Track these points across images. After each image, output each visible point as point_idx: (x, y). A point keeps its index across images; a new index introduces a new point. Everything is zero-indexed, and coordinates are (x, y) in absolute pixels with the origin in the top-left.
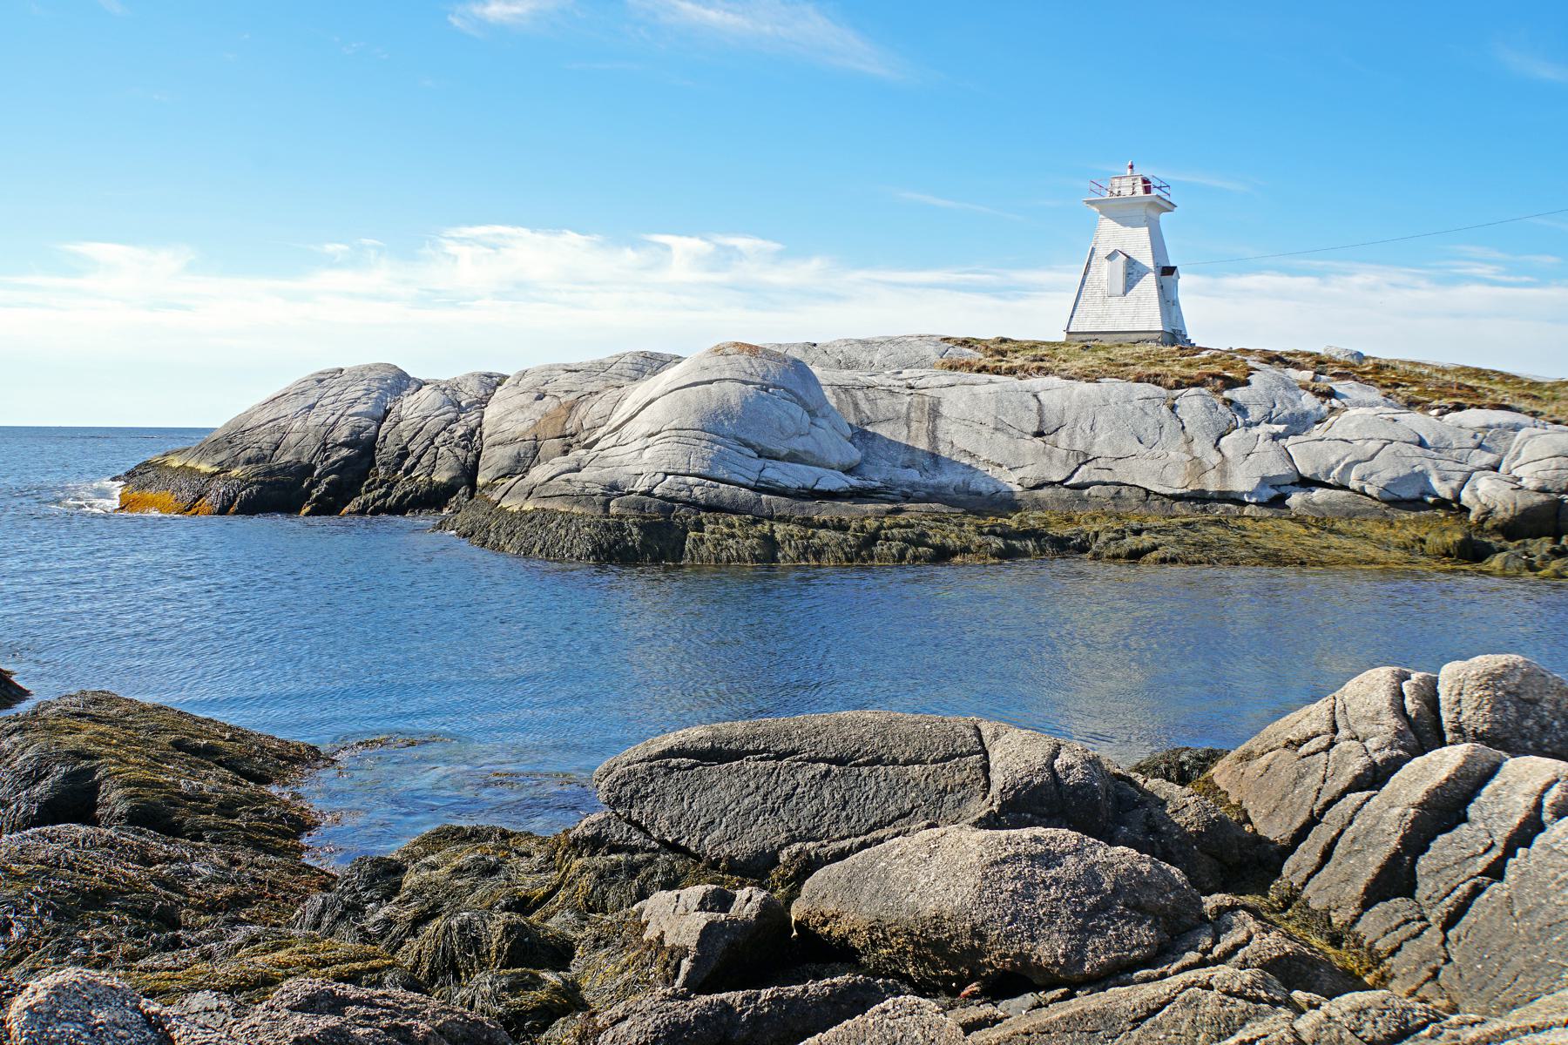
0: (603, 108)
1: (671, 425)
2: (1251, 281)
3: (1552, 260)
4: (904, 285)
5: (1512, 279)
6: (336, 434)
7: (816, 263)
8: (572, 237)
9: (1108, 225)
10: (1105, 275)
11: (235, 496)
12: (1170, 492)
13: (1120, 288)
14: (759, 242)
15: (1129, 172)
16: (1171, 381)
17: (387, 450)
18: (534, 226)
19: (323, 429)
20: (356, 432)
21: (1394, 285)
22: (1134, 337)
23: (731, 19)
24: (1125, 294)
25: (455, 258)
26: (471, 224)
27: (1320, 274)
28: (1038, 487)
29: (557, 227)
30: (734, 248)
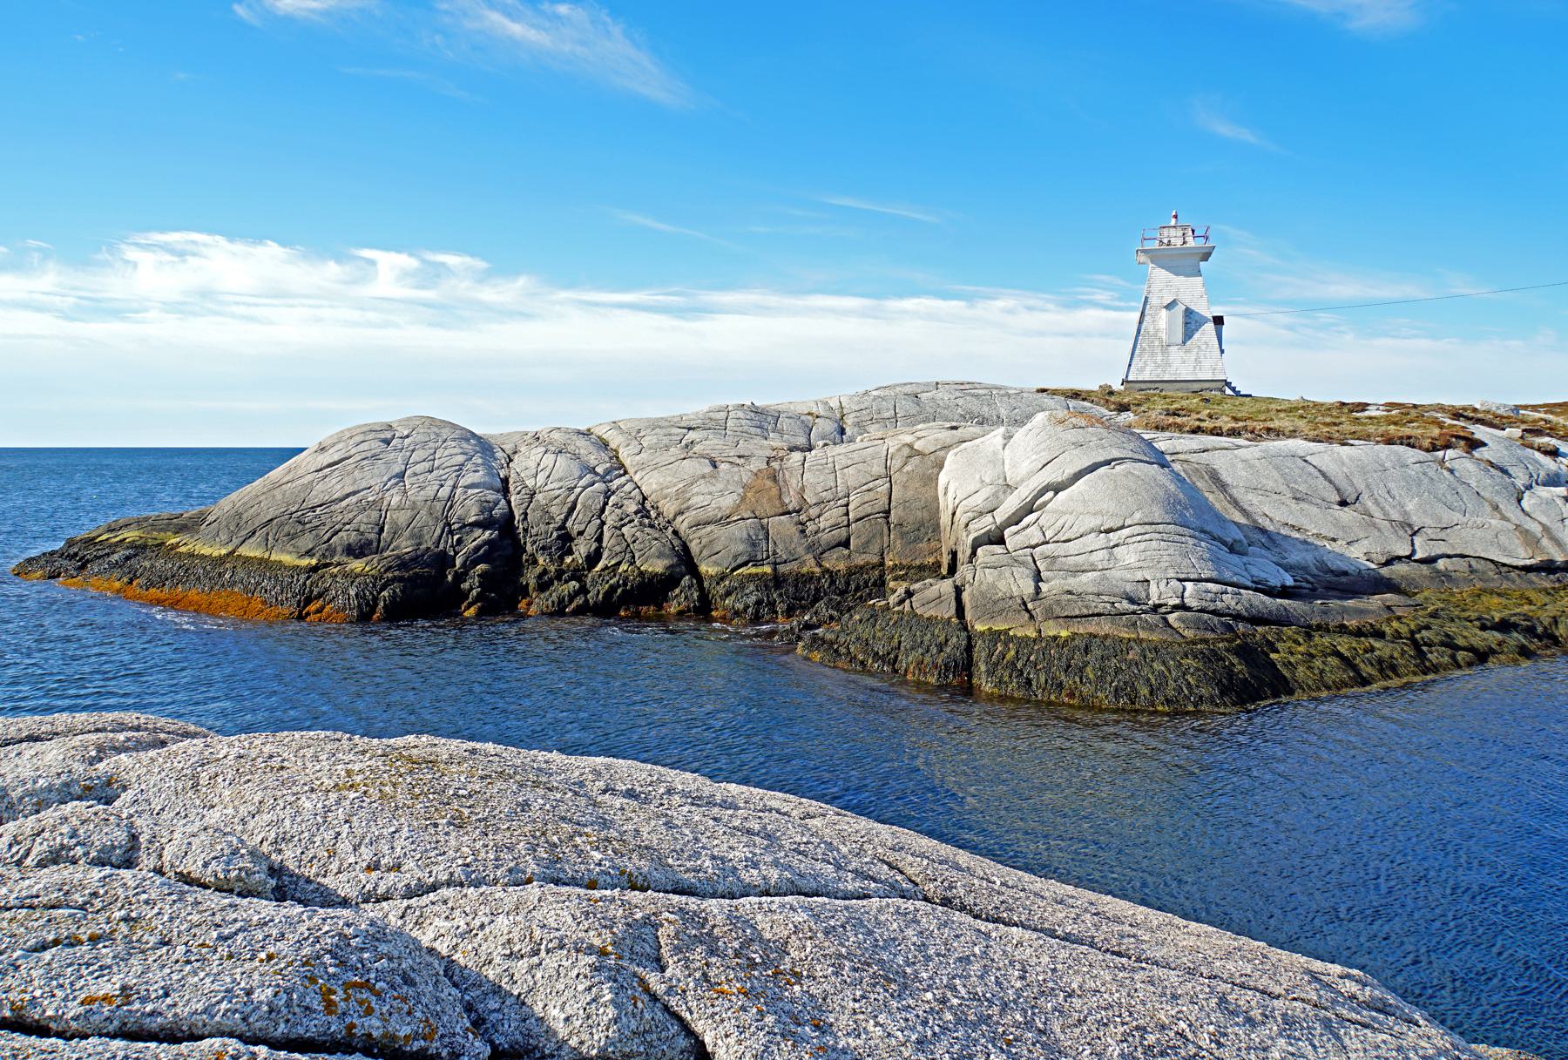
0: (379, 111)
1: (1138, 516)
2: (910, 304)
4: (596, 304)
6: (458, 511)
7: (522, 281)
8: (273, 249)
9: (1160, 275)
11: (376, 599)
12: (1521, 563)
13: (1179, 337)
14: (468, 259)
15: (1173, 222)
16: (1426, 443)
17: (535, 535)
18: (231, 237)
19: (439, 506)
20: (486, 507)
21: (1030, 309)
23: (533, 35)
24: (1184, 343)
25: (135, 265)
26: (163, 230)
27: (969, 298)
28: (1388, 563)
29: (259, 239)
30: (443, 264)
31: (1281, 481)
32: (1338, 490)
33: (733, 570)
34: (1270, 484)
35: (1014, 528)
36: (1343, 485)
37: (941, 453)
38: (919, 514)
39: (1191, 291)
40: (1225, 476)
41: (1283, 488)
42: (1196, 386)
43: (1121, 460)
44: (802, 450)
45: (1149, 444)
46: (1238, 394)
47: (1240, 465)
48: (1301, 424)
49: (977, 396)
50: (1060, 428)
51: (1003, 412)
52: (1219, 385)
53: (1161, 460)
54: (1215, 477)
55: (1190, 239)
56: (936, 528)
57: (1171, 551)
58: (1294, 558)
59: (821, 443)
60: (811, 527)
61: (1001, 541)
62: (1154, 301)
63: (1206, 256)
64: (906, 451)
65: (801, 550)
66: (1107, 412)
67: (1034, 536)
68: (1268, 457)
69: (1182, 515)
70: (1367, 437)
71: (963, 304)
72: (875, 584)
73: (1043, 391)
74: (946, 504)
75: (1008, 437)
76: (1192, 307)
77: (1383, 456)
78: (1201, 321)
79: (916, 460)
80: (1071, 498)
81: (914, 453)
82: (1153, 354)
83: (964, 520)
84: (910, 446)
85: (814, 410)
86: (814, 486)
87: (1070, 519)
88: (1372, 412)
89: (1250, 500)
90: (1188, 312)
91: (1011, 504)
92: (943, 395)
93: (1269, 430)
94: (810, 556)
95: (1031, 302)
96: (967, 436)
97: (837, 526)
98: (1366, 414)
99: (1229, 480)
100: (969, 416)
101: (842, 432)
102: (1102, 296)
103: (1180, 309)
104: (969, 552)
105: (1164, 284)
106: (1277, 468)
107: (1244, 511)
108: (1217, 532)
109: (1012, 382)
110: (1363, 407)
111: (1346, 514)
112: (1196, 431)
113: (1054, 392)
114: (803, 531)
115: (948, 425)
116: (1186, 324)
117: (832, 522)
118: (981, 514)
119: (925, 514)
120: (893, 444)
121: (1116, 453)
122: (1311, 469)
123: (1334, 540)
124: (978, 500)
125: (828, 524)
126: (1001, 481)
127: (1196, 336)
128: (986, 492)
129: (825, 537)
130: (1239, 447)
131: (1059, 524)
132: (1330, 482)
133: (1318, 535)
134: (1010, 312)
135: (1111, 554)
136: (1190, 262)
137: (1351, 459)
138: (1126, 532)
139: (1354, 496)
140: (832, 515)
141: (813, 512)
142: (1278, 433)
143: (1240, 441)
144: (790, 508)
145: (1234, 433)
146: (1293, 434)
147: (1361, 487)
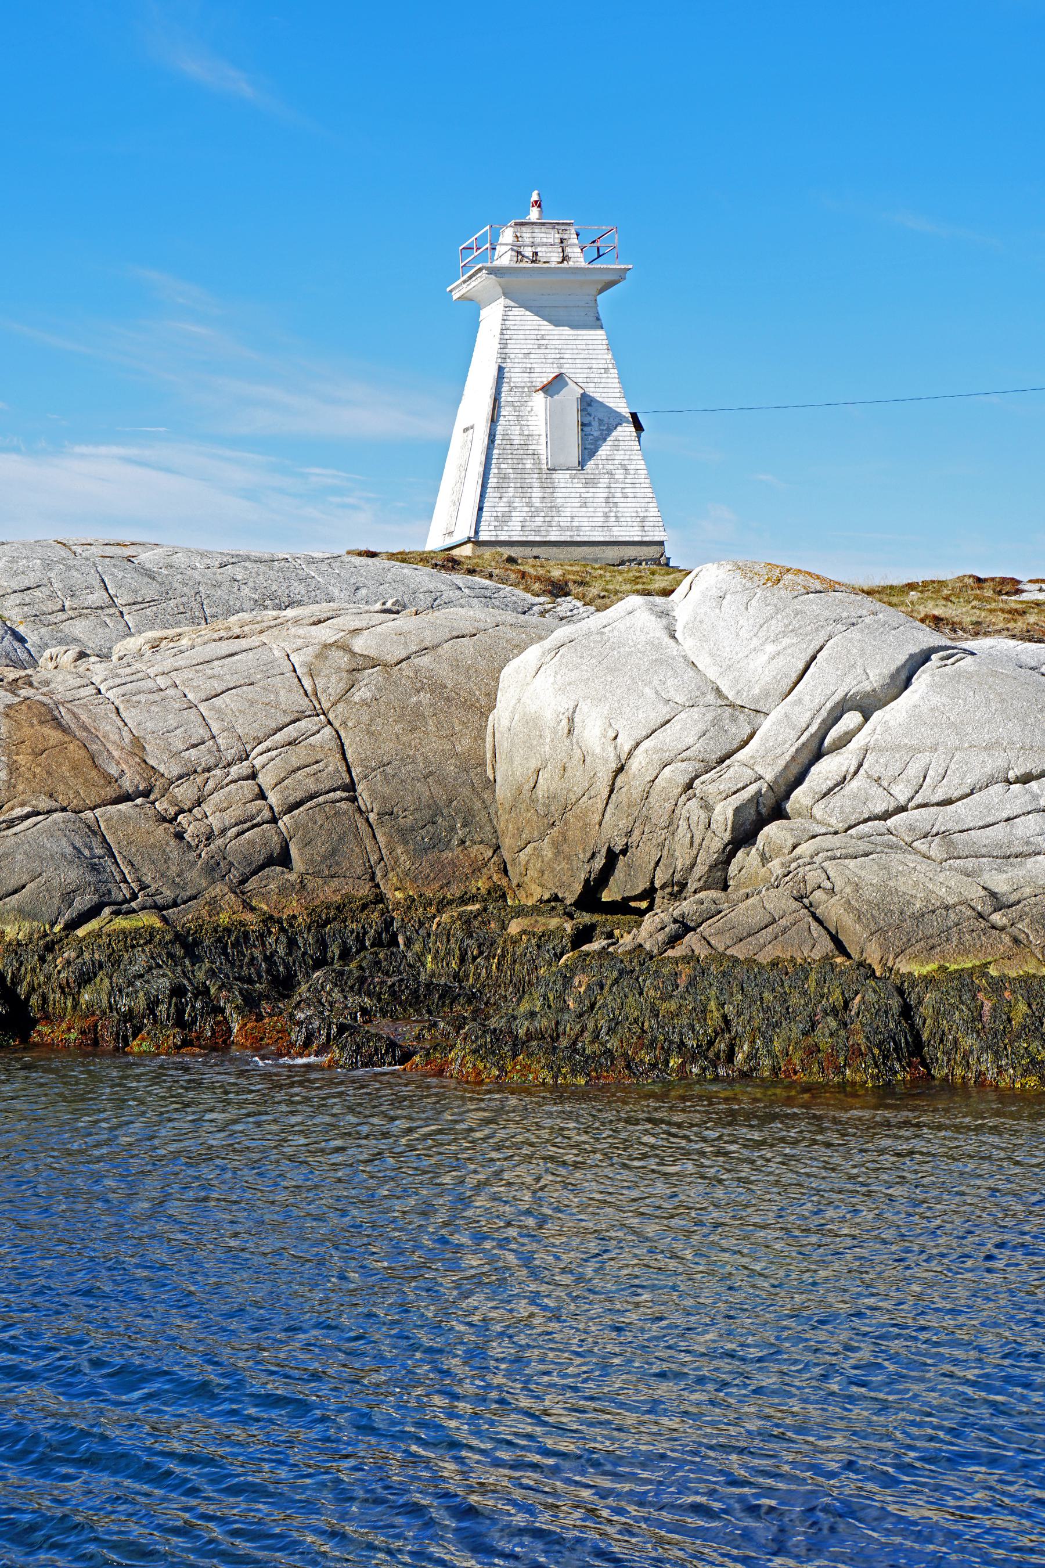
13: (573, 455)
15: (534, 215)
22: (612, 554)
24: (582, 464)
33: (73, 925)
55: (574, 252)
62: (515, 376)
64: (343, 660)
65: (195, 877)
72: (377, 943)
76: (592, 392)
78: (610, 421)
82: (524, 489)
90: (586, 402)
97: (247, 823)
103: (571, 394)
110: (1010, 586)
114: (179, 836)
117: (235, 813)
125: (229, 817)
127: (604, 451)
131: (914, 770)
141: (185, 792)
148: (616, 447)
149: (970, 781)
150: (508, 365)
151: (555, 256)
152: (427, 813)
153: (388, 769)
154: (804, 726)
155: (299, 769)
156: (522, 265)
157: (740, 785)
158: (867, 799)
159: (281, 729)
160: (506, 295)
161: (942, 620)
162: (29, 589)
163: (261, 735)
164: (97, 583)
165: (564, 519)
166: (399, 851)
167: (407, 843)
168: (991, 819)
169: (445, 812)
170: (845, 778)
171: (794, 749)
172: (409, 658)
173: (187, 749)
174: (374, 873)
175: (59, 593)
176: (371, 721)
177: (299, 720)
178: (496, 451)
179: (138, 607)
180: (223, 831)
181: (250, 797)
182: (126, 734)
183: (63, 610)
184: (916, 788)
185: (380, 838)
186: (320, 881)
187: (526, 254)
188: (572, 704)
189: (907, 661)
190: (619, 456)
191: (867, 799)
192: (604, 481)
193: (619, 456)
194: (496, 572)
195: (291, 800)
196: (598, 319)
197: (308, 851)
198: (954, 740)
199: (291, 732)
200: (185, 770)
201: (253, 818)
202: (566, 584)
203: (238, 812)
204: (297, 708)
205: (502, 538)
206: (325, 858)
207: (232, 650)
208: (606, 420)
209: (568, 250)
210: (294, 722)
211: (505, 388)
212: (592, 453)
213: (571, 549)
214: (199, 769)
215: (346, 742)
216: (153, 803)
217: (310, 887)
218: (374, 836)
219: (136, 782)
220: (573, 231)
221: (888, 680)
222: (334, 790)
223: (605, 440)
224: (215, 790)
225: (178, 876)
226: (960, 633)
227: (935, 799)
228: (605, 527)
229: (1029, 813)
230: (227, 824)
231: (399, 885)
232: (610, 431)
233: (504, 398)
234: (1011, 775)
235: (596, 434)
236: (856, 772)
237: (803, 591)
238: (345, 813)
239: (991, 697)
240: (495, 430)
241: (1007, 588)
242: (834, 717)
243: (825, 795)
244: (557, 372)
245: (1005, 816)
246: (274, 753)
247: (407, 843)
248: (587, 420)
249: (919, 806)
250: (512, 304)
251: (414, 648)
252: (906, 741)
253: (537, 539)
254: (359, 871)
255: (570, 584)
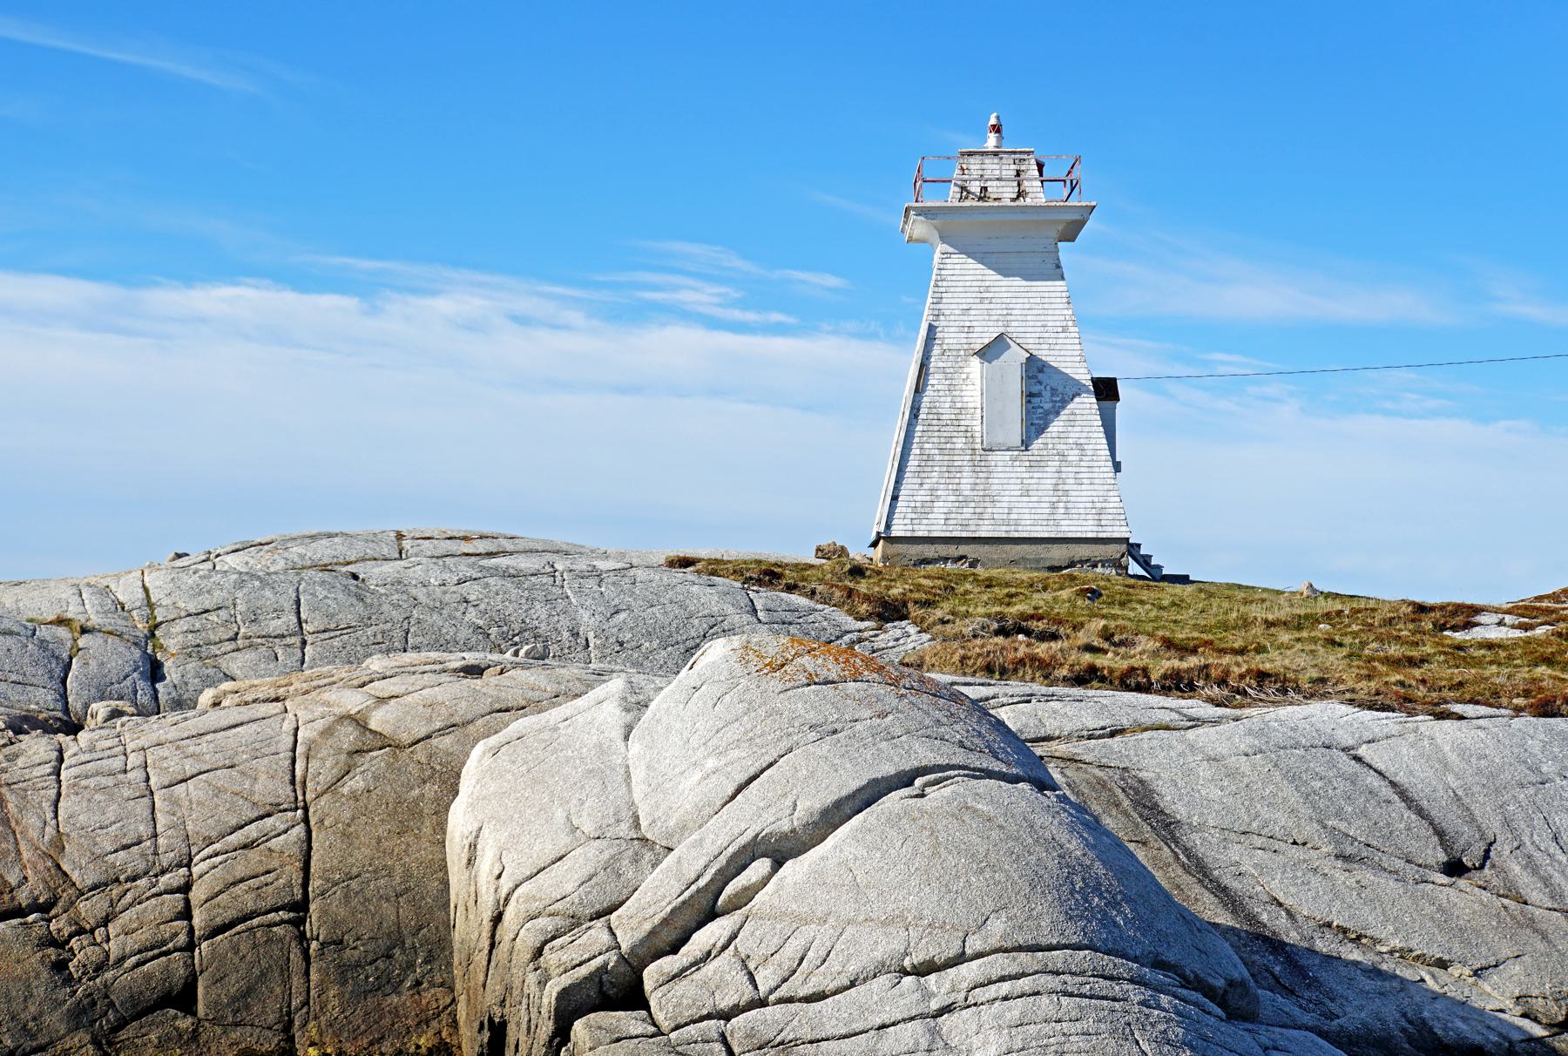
1: (997, 928)
3: (832, 281)
5: (751, 316)
9: (962, 274)
10: (972, 395)
13: (1015, 434)
15: (991, 141)
21: (522, 321)
24: (1026, 444)
27: (366, 289)
31: (1305, 811)
32: (1440, 834)
34: (1281, 821)
35: (669, 964)
36: (1451, 820)
37: (446, 742)
38: (387, 909)
39: (1042, 317)
40: (1168, 798)
41: (1310, 830)
42: (1058, 554)
43: (938, 772)
44: (47, 728)
45: (979, 708)
46: (1155, 575)
47: (1205, 771)
48: (1334, 659)
49: (506, 574)
50: (774, 683)
51: (587, 622)
52: (1114, 551)
53: (1024, 763)
54: (1144, 801)
55: (1032, 185)
56: (439, 947)
57: (1088, 1024)
58: (1355, 1014)
59: (100, 709)
60: (83, 953)
61: (630, 996)
62: (949, 337)
63: (1071, 232)
64: (348, 736)
66: (850, 623)
67: (724, 982)
68: (1270, 749)
69: (1107, 923)
70: (1492, 698)
71: (349, 303)
73: (685, 563)
74: (472, 888)
75: (636, 705)
76: (1043, 354)
77: (1535, 746)
78: (1065, 392)
79: (377, 760)
80: (817, 877)
81: (372, 742)
82: (951, 470)
83: (529, 938)
84: (359, 721)
85: (72, 612)
86: (89, 833)
87: (821, 937)
88: (1488, 630)
89: (1237, 861)
90: (1035, 369)
91: (656, 894)
92: (421, 571)
93: (1262, 676)
94: (83, 1036)
95: (524, 305)
96: (513, 697)
97: (157, 948)
98: (1477, 634)
99: (1180, 811)
100: (504, 634)
101: (155, 672)
102: (699, 296)
103: (1014, 359)
104: (546, 1028)
105: (971, 295)
106: (1293, 778)
107: (1222, 892)
108: (1193, 966)
109: (608, 542)
110: (1466, 615)
111: (1463, 897)
112: (1086, 677)
113: (715, 568)
114: (60, 966)
115: (455, 660)
116: (1030, 396)
117: (143, 936)
118: (575, 922)
119: (406, 912)
120: (309, 715)
121: (924, 754)
122: (1372, 780)
123: (1443, 964)
124: (564, 882)
125: (132, 943)
126: (624, 829)
127: (1055, 427)
128: (585, 859)
129: (122, 980)
130: (1196, 722)
132: (1421, 812)
133: (1404, 954)
134: (473, 326)
135: (934, 1032)
136: (1028, 243)
137: (1462, 752)
138: (969, 972)
139: (1478, 849)
140: (139, 922)
141: (90, 909)
142: (1281, 686)
143: (1197, 707)
144: (23, 897)
145: (1178, 684)
146: (1319, 689)
147: (1494, 826)
148: (1071, 423)
149: (853, 968)
150: (941, 323)
151: (1009, 191)
152: (383, 943)
153: (354, 884)
154: (693, 876)
155: (242, 880)
156: (967, 203)
157: (586, 956)
158: (717, 987)
159: (242, 827)
160: (943, 239)
161: (1269, 675)
162: (207, 611)
163: (214, 834)
164: (289, 605)
165: (999, 511)
166: (331, 993)
167: (344, 983)
168: (857, 1026)
169: (408, 943)
170: (709, 953)
171: (669, 909)
172: (429, 737)
173: (116, 851)
174: (291, 1022)
175: (239, 617)
176: (353, 819)
177: (269, 815)
178: (919, 428)
179: (327, 635)
180: (121, 960)
181: (168, 914)
182: (50, 831)
183: (234, 638)
184: (786, 974)
185: (314, 976)
186: (219, 1030)
187: (972, 190)
188: (476, 826)
189: (859, 790)
190: (1075, 434)
191: (717, 987)
192: (1053, 465)
193: (1075, 434)
194: (820, 588)
195: (219, 921)
196: (1058, 266)
197: (214, 991)
198: (848, 911)
199: (252, 831)
200: (103, 878)
201: (164, 943)
202: (905, 604)
203: (147, 935)
204: (272, 800)
205: (920, 534)
206: (234, 999)
207: (239, 719)
208: (1060, 389)
209: (1026, 183)
210: (261, 818)
211: (936, 351)
212: (1041, 430)
213: (1008, 547)
214: (122, 878)
215: (315, 845)
216: (50, 920)
217: (204, 1037)
218: (307, 973)
219: (36, 893)
220: (1033, 162)
221: (816, 818)
222: (277, 910)
223: (1058, 414)
224: (131, 905)
225: (34, 1019)
226: (1292, 694)
227: (801, 994)
228: (1051, 518)
229: (912, 1019)
230: (128, 950)
231: (317, 1039)
232: (1065, 402)
233: (934, 363)
234: (907, 963)
235: (1047, 406)
236: (725, 947)
237: (805, 681)
238: (281, 940)
239: (923, 848)
240: (920, 402)
241: (1460, 619)
242: (739, 863)
243: (674, 977)
244: (1002, 330)
245: (878, 1022)
246: (219, 859)
247: (344, 983)
248: (1035, 389)
249: (780, 1001)
250: (951, 250)
251: (438, 725)
252: (794, 907)
253: (964, 534)
254: (271, 1018)
255: (910, 605)
